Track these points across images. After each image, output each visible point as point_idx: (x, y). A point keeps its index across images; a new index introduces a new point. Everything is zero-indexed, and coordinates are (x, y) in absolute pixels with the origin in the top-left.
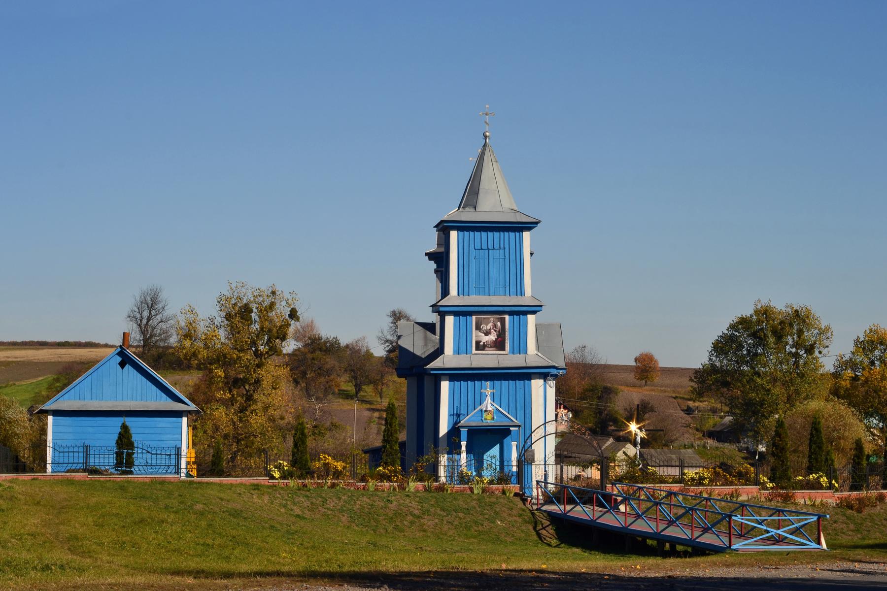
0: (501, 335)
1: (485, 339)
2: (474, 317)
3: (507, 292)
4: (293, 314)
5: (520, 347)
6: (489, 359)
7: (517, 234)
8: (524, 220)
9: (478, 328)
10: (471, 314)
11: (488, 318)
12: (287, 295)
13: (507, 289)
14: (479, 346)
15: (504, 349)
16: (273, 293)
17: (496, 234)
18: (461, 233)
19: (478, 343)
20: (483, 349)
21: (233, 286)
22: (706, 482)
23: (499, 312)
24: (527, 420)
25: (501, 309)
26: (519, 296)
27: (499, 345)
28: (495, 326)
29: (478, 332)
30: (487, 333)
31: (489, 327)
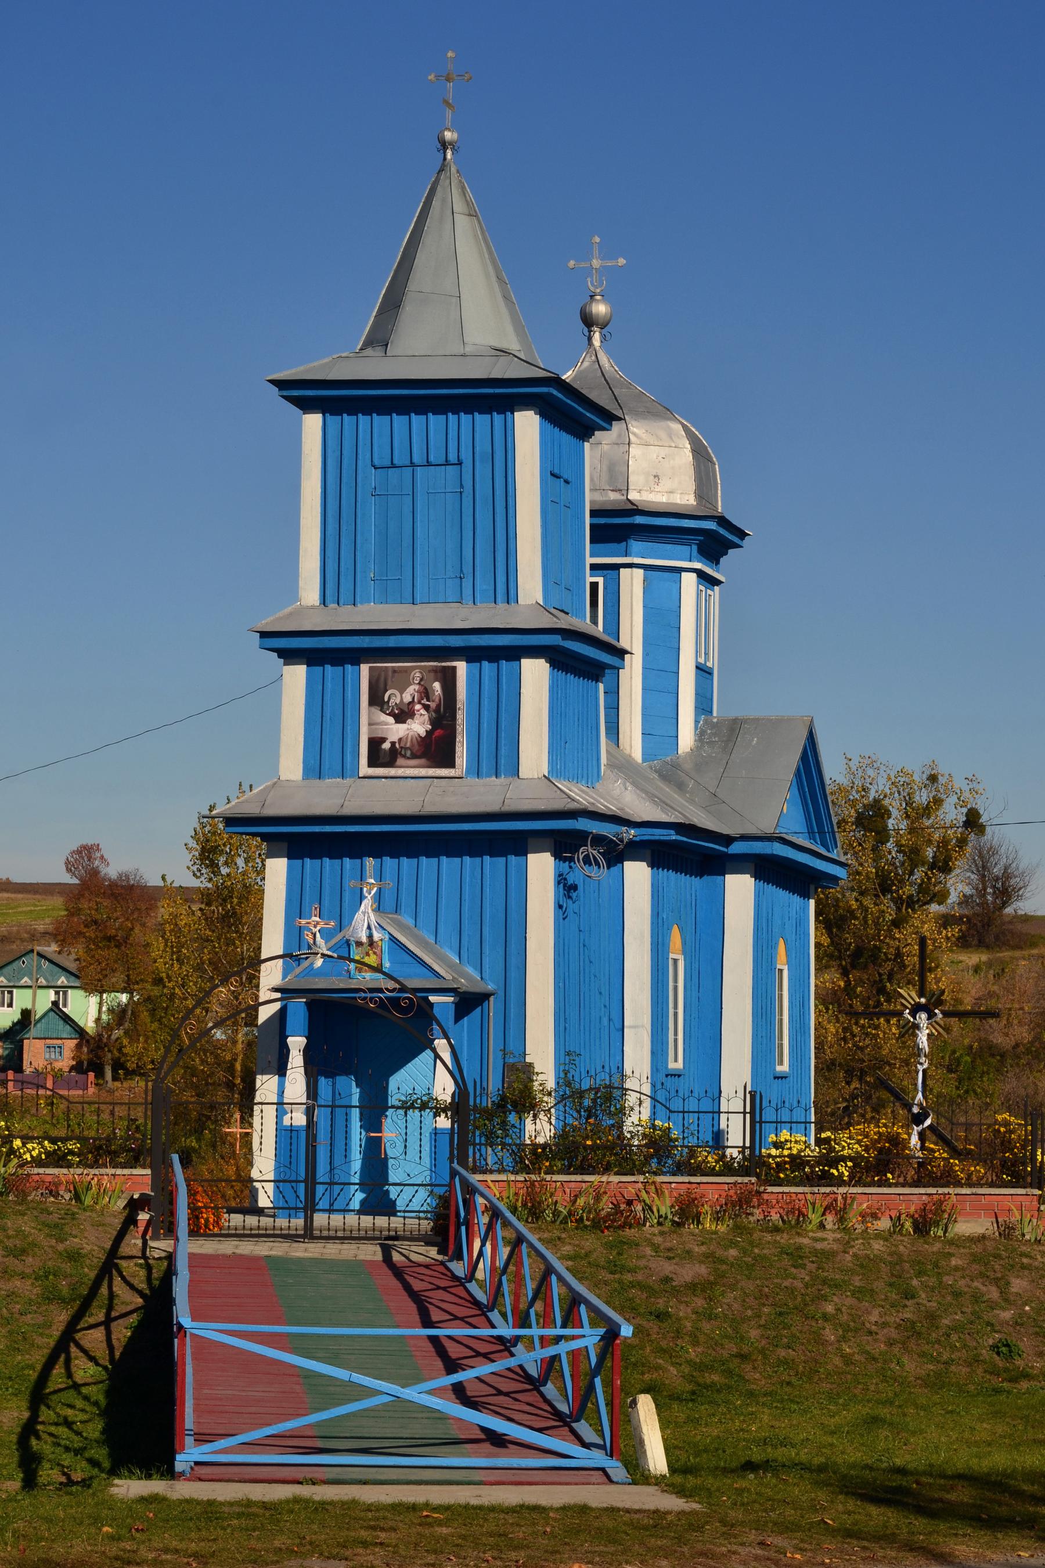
0: (444, 719)
1: (395, 732)
2: (365, 668)
3: (468, 591)
4: (973, 821)
5: (501, 755)
6: (409, 791)
7: (498, 418)
8: (496, 374)
9: (376, 700)
10: (355, 656)
11: (407, 671)
12: (959, 783)
13: (467, 583)
14: (382, 755)
15: (451, 764)
16: (933, 778)
17: (435, 421)
18: (333, 420)
19: (375, 743)
20: (391, 763)
21: (853, 765)
22: (844, 1170)
23: (437, 650)
24: (513, 974)
25: (438, 641)
26: (502, 606)
27: (437, 749)
28: (426, 693)
29: (376, 710)
30: (402, 715)
31: (407, 698)
